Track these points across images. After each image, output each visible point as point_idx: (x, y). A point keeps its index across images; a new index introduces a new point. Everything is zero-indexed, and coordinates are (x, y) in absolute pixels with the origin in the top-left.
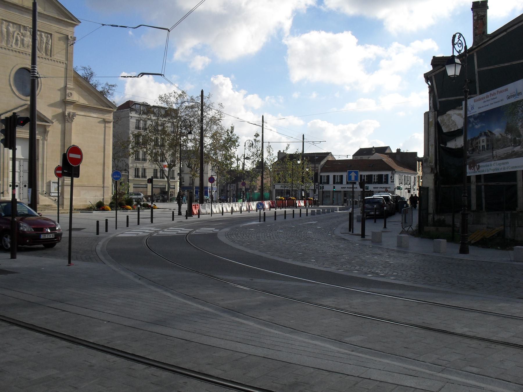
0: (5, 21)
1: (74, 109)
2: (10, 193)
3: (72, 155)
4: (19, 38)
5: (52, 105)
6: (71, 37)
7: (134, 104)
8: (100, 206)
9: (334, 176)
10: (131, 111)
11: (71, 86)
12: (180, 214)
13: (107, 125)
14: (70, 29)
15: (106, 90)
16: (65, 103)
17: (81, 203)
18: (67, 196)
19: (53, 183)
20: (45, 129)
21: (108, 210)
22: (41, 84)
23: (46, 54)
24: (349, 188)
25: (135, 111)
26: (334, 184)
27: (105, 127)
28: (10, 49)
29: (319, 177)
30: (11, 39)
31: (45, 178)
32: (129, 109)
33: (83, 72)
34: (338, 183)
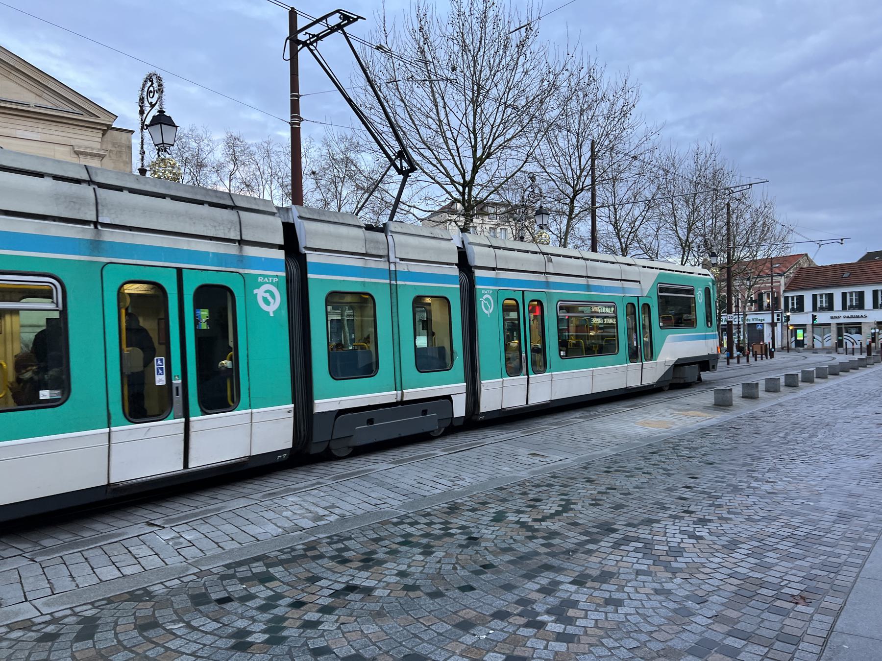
2: (125, 431)
9: (844, 295)
24: (848, 317)
26: (813, 311)
29: (782, 300)
34: (822, 309)
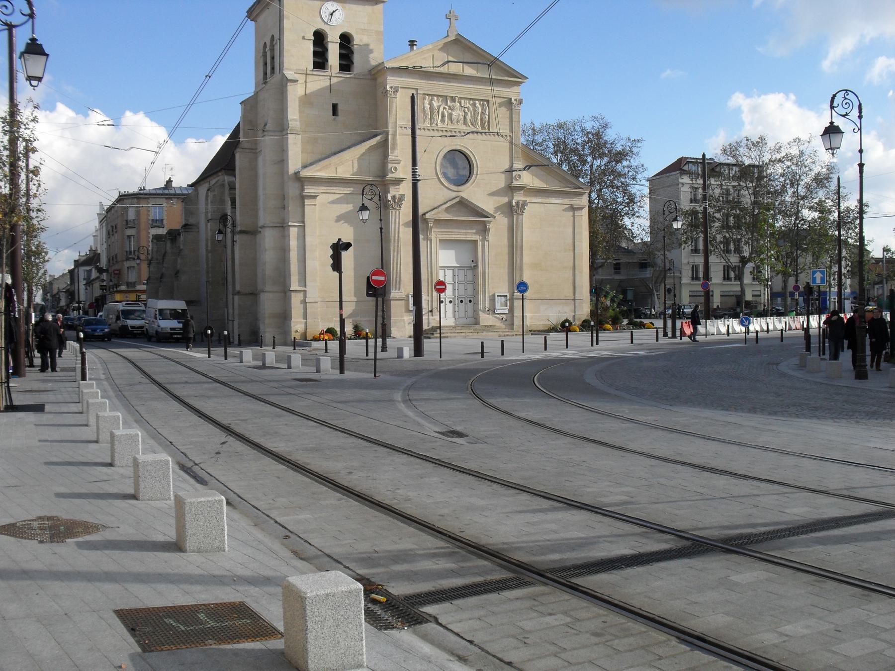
0: (428, 95)
1: (525, 195)
3: (374, 278)
4: (446, 114)
5: (493, 194)
6: (516, 100)
7: (686, 164)
8: (565, 327)
10: (681, 174)
11: (519, 166)
12: (665, 335)
13: (576, 213)
14: (515, 89)
15: (628, 148)
16: (511, 189)
17: (542, 323)
18: (518, 313)
19: (498, 296)
20: (486, 226)
21: (576, 331)
22: (477, 167)
23: (483, 127)
25: (687, 174)
27: (574, 216)
28: (435, 129)
30: (436, 117)
31: (487, 290)
32: (678, 172)
33: (593, 123)
